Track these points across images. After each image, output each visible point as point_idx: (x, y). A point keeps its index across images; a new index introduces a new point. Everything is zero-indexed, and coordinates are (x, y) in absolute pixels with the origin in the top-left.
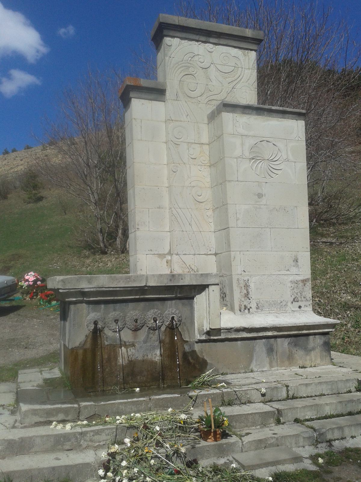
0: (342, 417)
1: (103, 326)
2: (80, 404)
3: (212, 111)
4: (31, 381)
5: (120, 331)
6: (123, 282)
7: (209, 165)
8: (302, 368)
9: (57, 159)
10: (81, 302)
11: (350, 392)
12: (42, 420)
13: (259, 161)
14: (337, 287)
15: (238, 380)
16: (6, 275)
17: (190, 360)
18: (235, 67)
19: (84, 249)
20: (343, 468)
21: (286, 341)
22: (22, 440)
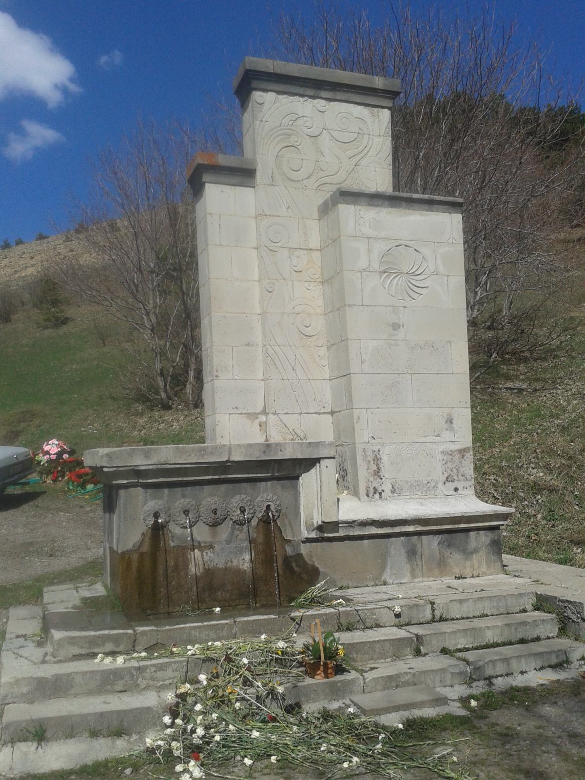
0: (510, 646)
1: (167, 520)
2: (136, 629)
3: (325, 201)
4: (62, 601)
5: (191, 527)
6: (196, 455)
7: (321, 280)
8: (459, 578)
9: (89, 259)
10: (135, 485)
11: (524, 611)
12: (83, 651)
13: (393, 277)
14: (524, 459)
15: (364, 596)
16: (13, 446)
17: (294, 568)
18: (359, 133)
19: (136, 401)
20: (504, 713)
21: (435, 540)
22: (58, 678)
